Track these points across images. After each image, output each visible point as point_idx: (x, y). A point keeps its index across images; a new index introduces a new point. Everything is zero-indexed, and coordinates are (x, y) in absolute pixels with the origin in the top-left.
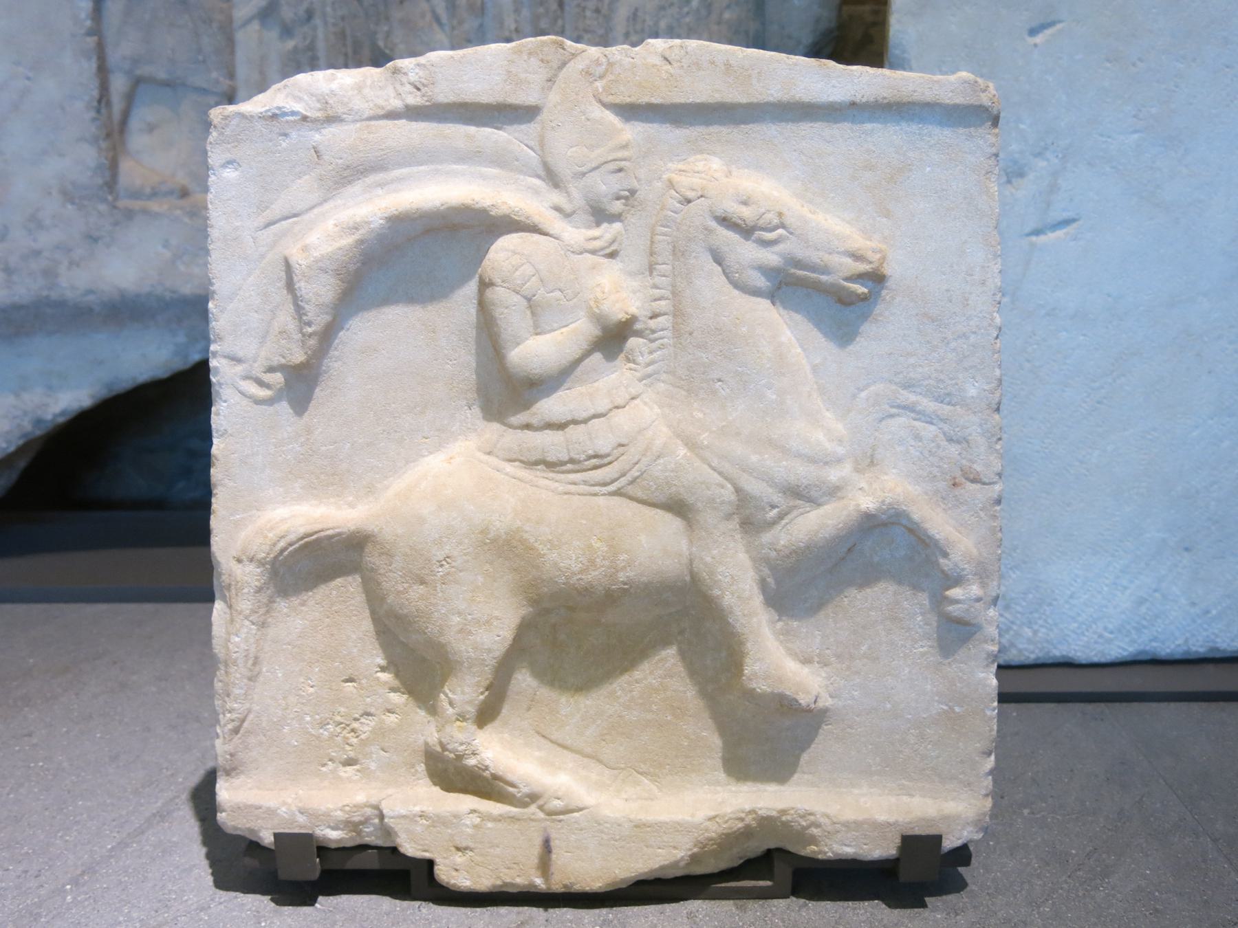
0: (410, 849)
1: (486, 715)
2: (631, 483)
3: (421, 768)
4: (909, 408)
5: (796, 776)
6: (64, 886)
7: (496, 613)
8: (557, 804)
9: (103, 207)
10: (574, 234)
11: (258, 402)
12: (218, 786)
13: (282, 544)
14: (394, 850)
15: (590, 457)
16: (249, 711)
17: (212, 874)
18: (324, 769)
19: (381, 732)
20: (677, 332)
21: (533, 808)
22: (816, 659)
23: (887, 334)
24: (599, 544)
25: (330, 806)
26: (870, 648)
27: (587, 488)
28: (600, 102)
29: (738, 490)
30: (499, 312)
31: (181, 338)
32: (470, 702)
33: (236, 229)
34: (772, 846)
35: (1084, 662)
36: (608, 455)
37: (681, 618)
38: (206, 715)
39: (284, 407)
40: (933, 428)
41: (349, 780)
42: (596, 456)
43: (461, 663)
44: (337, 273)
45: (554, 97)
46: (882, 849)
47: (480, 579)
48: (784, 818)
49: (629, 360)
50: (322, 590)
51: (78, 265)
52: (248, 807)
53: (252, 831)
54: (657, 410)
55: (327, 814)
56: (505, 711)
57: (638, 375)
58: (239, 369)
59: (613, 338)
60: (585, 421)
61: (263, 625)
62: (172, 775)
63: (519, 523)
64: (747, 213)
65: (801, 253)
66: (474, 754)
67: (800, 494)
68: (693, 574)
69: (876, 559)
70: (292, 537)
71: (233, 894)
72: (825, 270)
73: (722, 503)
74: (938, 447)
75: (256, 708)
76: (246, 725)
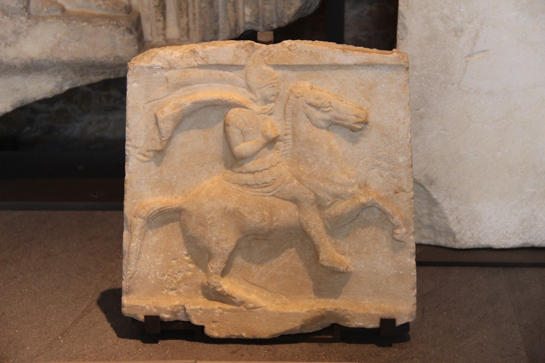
0: (195, 322)
1: (224, 273)
2: (279, 191)
3: (200, 292)
4: (378, 166)
5: (341, 296)
6: (58, 337)
7: (229, 237)
8: (251, 305)
9: (23, 18)
10: (256, 108)
11: (143, 161)
12: (122, 298)
13: (151, 212)
14: (189, 323)
15: (263, 183)
16: (136, 271)
17: (116, 332)
18: (163, 292)
19: (185, 279)
20: (294, 140)
21: (242, 307)
22: (347, 254)
23: (370, 140)
24: (266, 213)
25: (166, 306)
26: (367, 249)
27: (262, 194)
28: (266, 64)
29: (316, 195)
30: (231, 135)
31: (59, 79)
32: (219, 268)
33: (137, 104)
34: (333, 322)
35: (266, 336)
36: (269, 183)
37: (299, 237)
38: (92, 268)
39: (153, 164)
40: (387, 173)
41: (173, 296)
42: (265, 183)
43: (216, 255)
44: (174, 120)
45: (250, 62)
46: (374, 324)
47: (223, 225)
48: (336, 312)
49: (277, 149)
50: (165, 227)
51: (10, 46)
52: (134, 306)
53: (135, 315)
54: (287, 167)
55: (164, 309)
56: (232, 271)
57: (280, 154)
58: (137, 151)
59: (271, 143)
60: (261, 171)
61: (143, 240)
62: (86, 295)
63: (238, 206)
64: (318, 102)
65: (337, 115)
66: (220, 287)
67: (337, 197)
68: (300, 224)
69: (368, 218)
70: (156, 209)
71: (126, 340)
72: (346, 120)
73: (311, 199)
74: (389, 179)
75: (139, 269)
76: (135, 275)
